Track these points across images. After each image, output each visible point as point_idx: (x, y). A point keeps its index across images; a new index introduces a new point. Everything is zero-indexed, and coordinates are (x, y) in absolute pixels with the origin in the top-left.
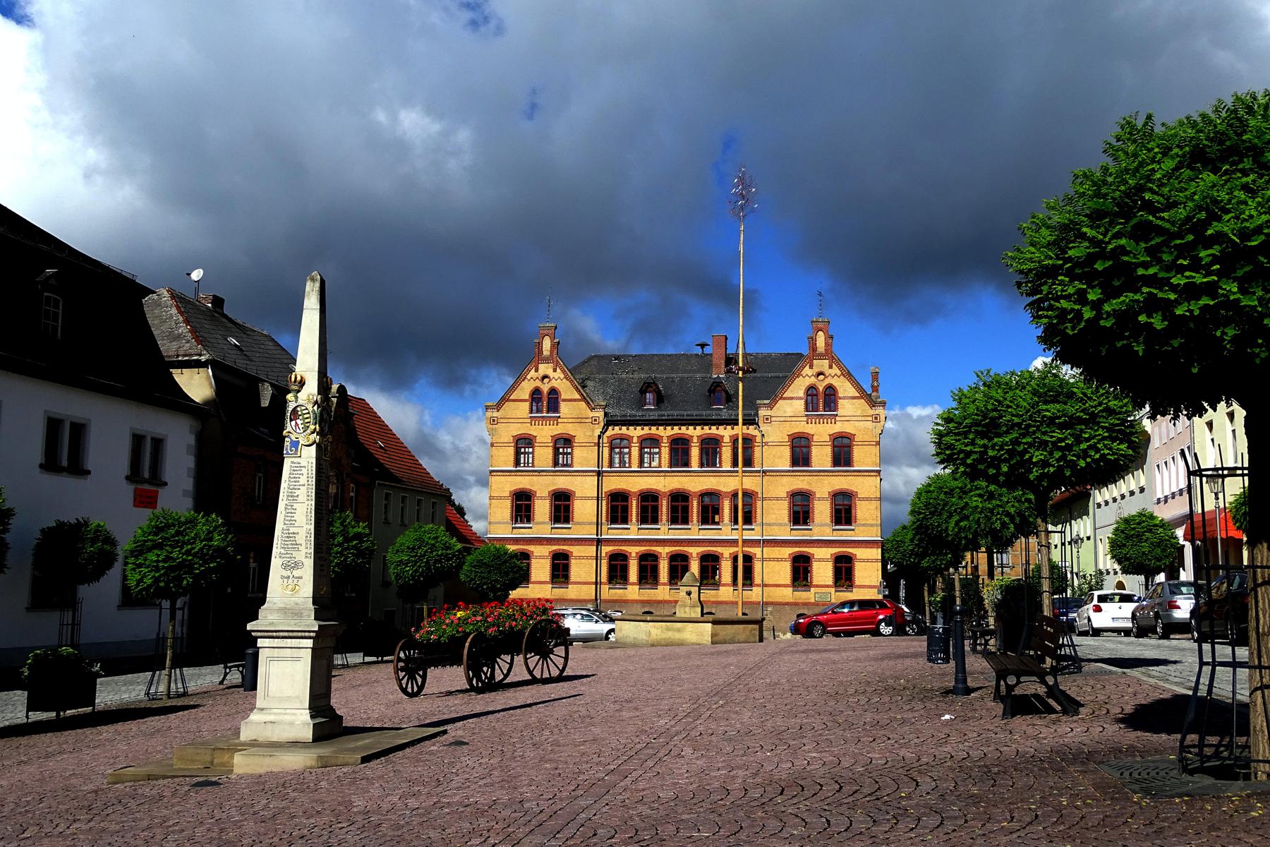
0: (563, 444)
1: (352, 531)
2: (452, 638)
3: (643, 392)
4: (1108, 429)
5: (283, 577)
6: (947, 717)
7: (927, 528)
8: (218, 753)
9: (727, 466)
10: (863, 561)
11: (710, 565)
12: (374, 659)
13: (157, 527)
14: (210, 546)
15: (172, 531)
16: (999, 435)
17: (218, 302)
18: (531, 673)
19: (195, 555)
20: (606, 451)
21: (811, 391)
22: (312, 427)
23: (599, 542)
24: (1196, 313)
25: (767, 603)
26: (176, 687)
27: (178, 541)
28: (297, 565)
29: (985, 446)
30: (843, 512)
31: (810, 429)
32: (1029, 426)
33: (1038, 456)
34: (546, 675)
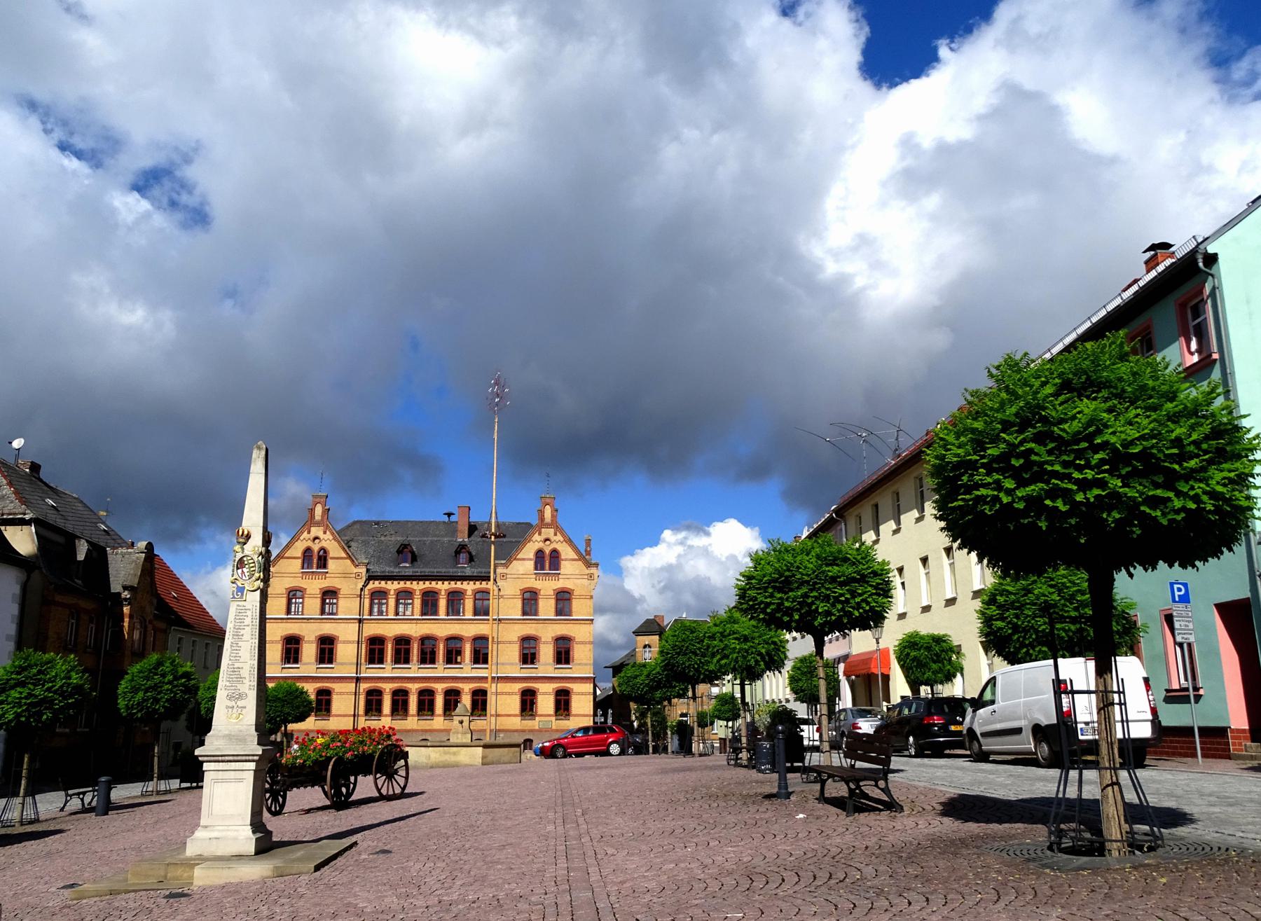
0: (329, 594)
1: (181, 670)
2: (316, 762)
3: (457, 553)
4: (876, 587)
5: (227, 707)
6: (801, 816)
7: (673, 666)
8: (171, 869)
9: (469, 615)
10: (579, 694)
11: (452, 698)
12: (188, 785)
13: (20, 667)
14: (69, 684)
15: (35, 671)
16: (792, 590)
17: (35, 467)
18: (379, 790)
19: (55, 692)
20: (367, 602)
21: (540, 554)
22: (257, 575)
23: (358, 680)
24: (1092, 500)
25: (500, 731)
26: (29, 814)
27: (40, 680)
28: (241, 696)
29: (781, 598)
30: (563, 655)
31: (537, 584)
32: (815, 583)
33: (822, 607)
34: (391, 792)
